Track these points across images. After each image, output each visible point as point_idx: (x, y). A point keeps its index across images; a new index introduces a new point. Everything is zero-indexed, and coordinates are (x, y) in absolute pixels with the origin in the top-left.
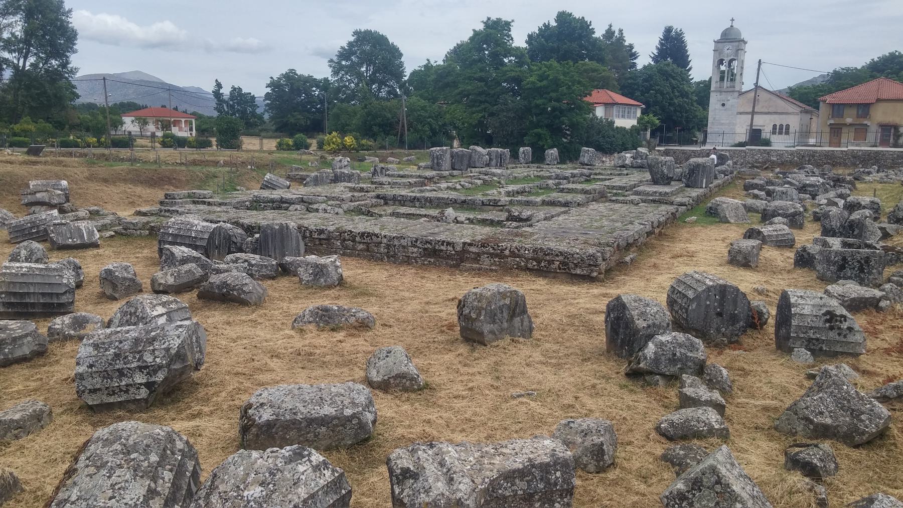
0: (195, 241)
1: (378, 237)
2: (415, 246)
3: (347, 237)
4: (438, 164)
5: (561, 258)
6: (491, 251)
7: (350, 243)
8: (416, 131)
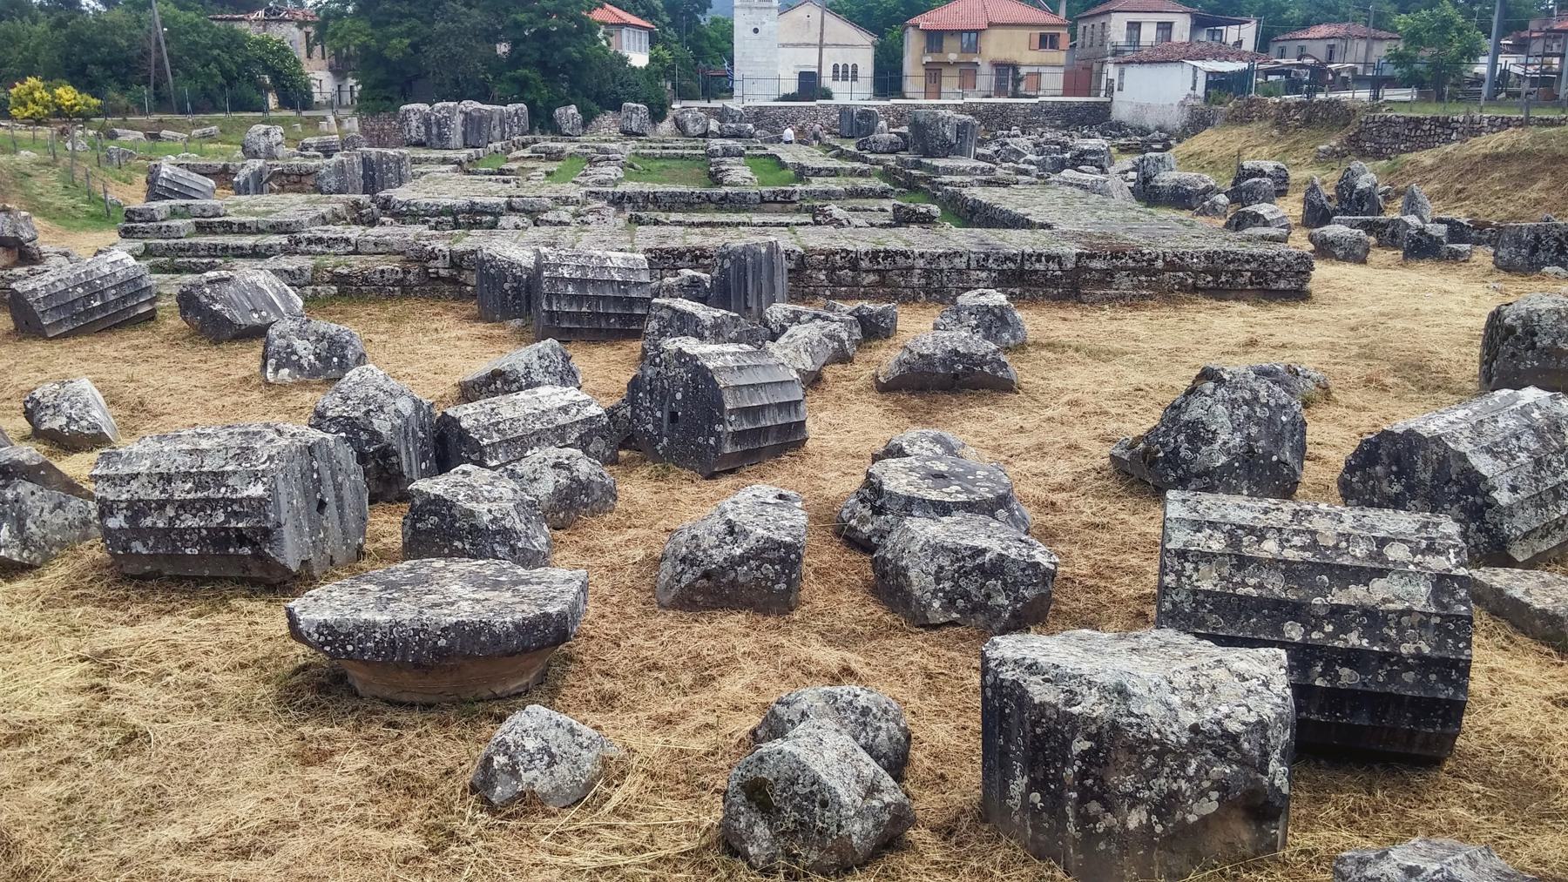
0: (626, 291)
1: (908, 257)
2: (982, 268)
3: (839, 263)
4: (440, 136)
5: (1254, 265)
6: (1131, 264)
7: (847, 274)
8: (190, 75)
